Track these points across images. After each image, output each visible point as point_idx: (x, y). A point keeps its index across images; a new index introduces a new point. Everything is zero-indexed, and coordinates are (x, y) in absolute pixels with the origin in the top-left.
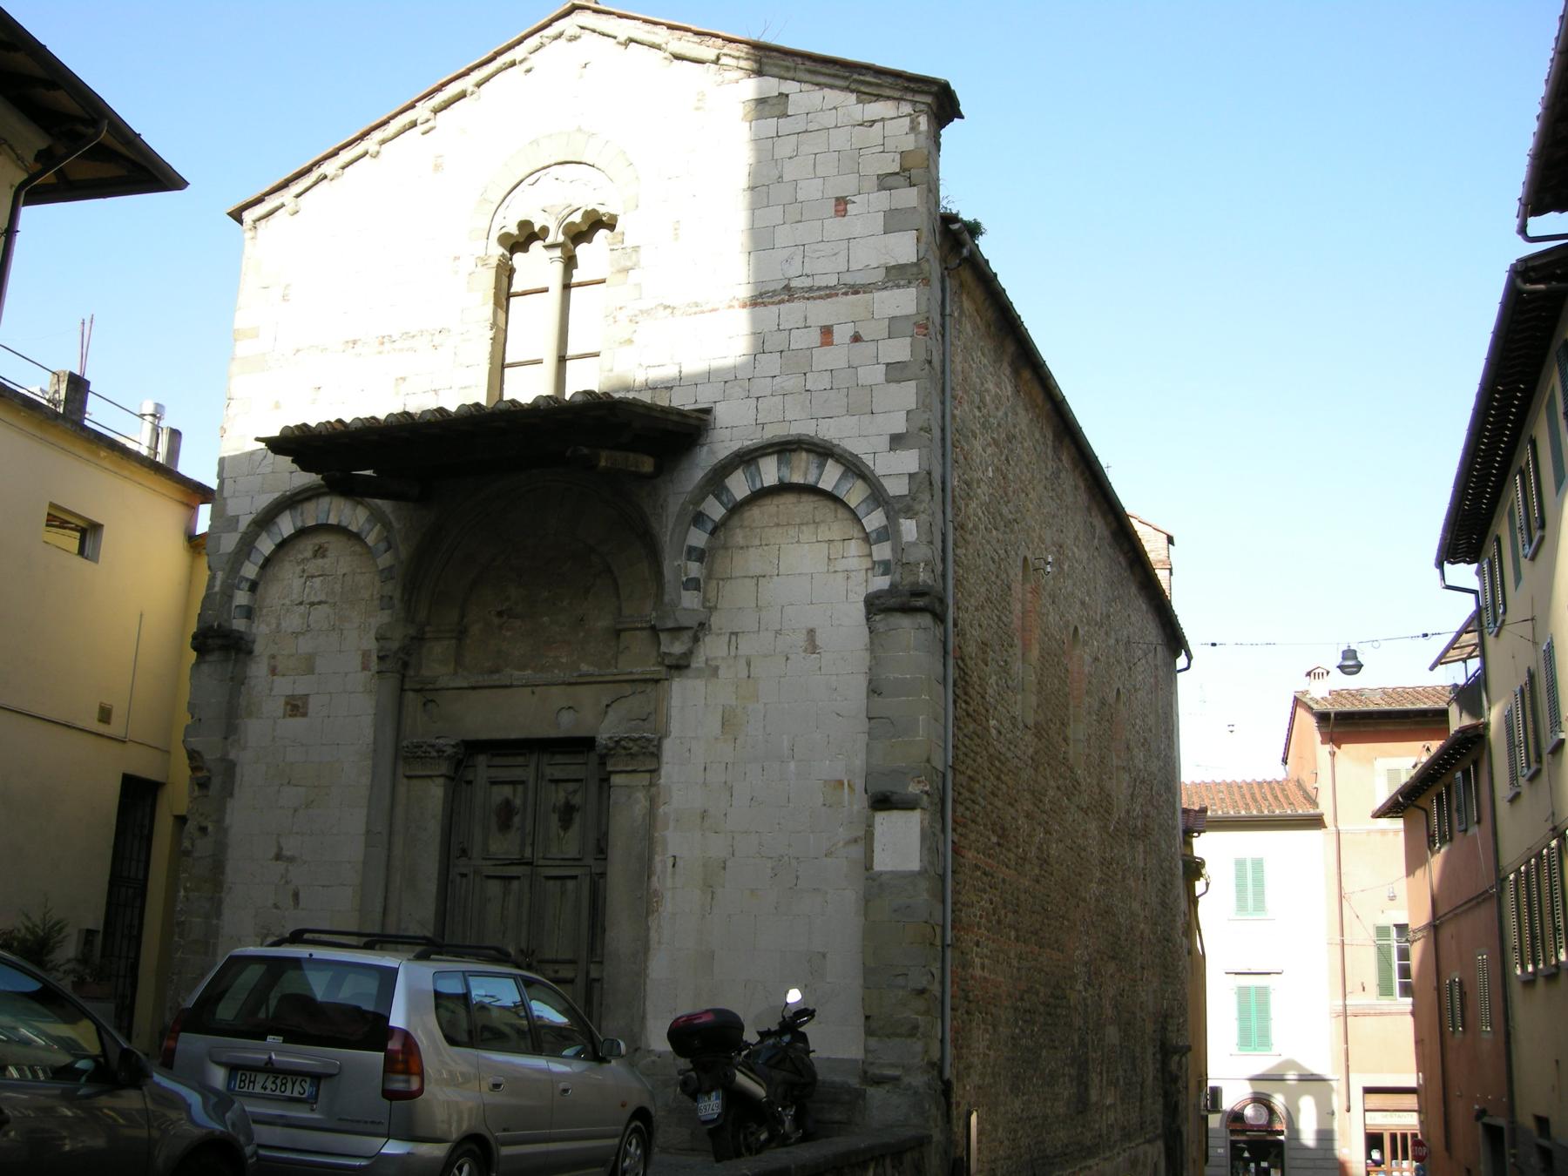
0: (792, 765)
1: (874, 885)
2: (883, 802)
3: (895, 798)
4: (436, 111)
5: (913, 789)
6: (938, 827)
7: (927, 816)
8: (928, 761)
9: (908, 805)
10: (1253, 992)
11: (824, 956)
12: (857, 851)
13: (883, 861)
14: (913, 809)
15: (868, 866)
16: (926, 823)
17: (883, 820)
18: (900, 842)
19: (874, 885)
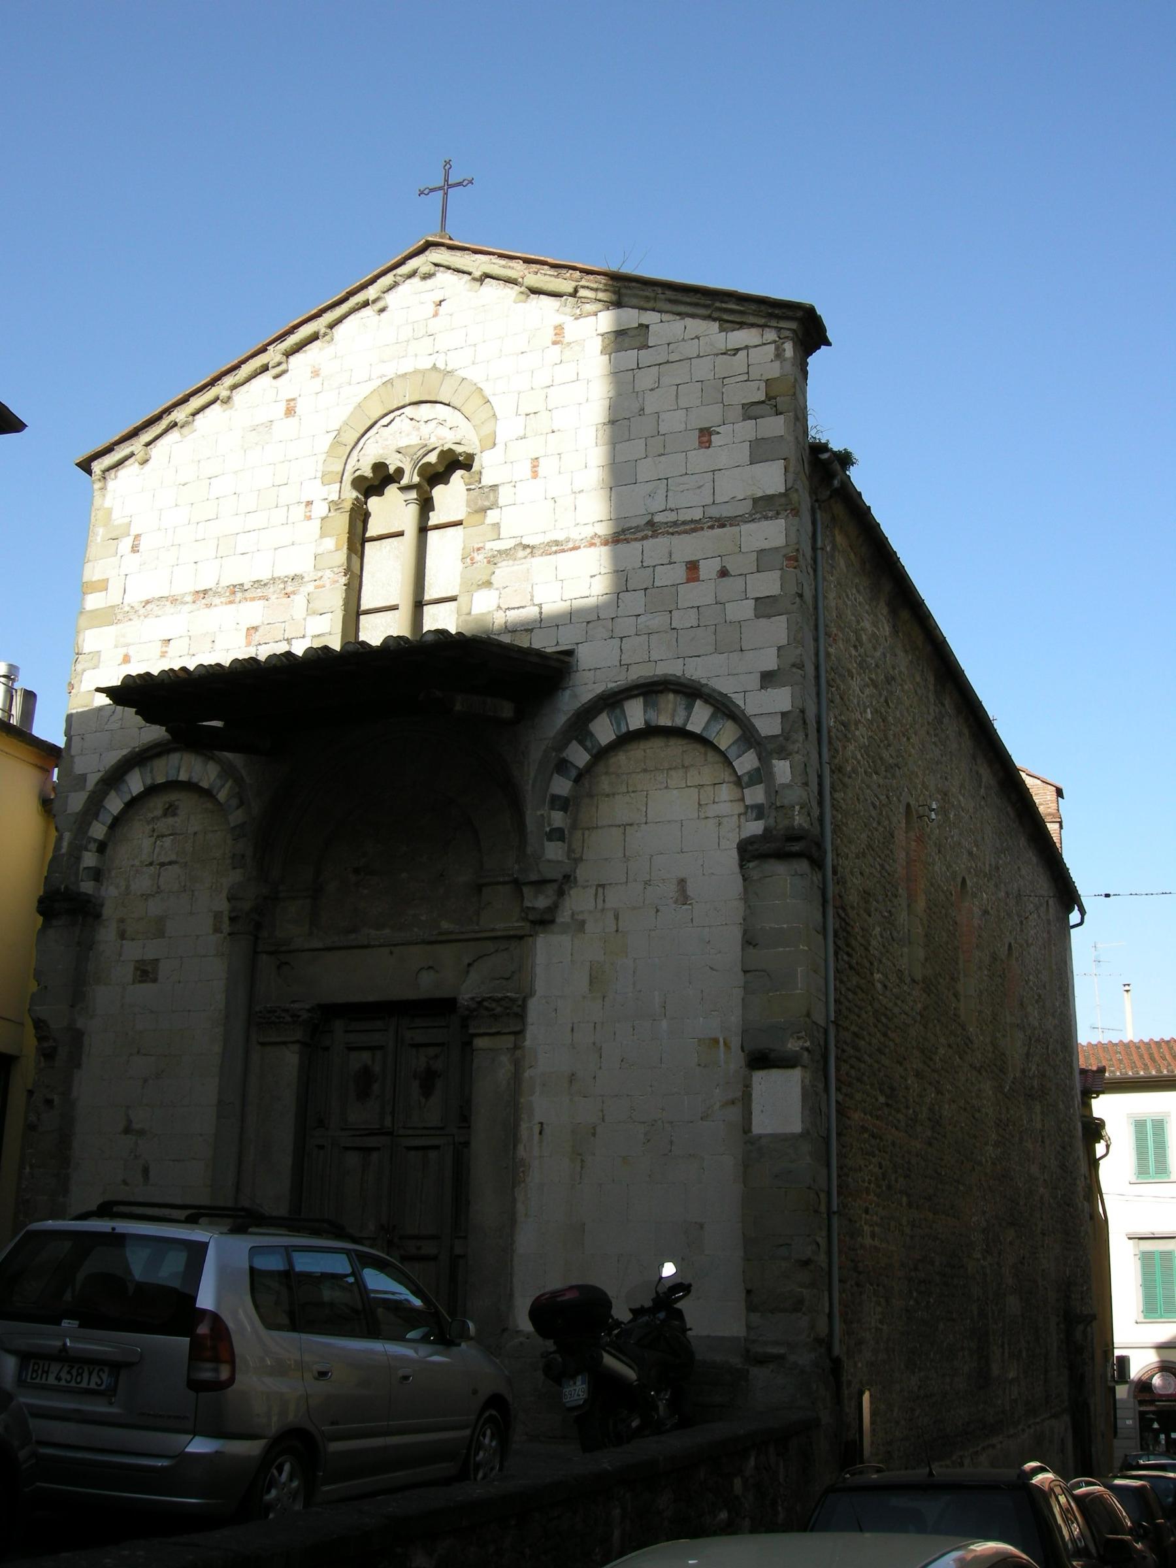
0: (664, 1024)
1: (754, 1150)
2: (760, 1060)
5: (793, 1045)
8: (808, 1015)
9: (786, 1062)
11: (701, 1226)
13: (762, 1125)
14: (793, 1066)
15: (747, 1129)
16: (807, 1081)
17: (765, 1082)
19: (754, 1150)
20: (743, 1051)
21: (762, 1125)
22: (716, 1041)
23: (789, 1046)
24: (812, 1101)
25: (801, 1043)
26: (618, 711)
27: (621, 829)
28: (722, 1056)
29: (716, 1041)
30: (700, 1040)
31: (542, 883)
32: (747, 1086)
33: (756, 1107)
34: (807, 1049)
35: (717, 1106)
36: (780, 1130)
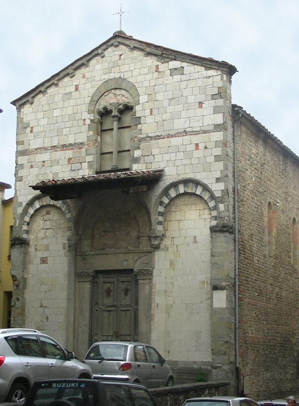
1: (213, 312)
2: (215, 288)
3: (218, 287)
5: (224, 284)
6: (232, 294)
9: (222, 288)
12: (209, 302)
14: (224, 290)
15: (212, 307)
18: (221, 299)
19: (213, 312)
22: (204, 282)
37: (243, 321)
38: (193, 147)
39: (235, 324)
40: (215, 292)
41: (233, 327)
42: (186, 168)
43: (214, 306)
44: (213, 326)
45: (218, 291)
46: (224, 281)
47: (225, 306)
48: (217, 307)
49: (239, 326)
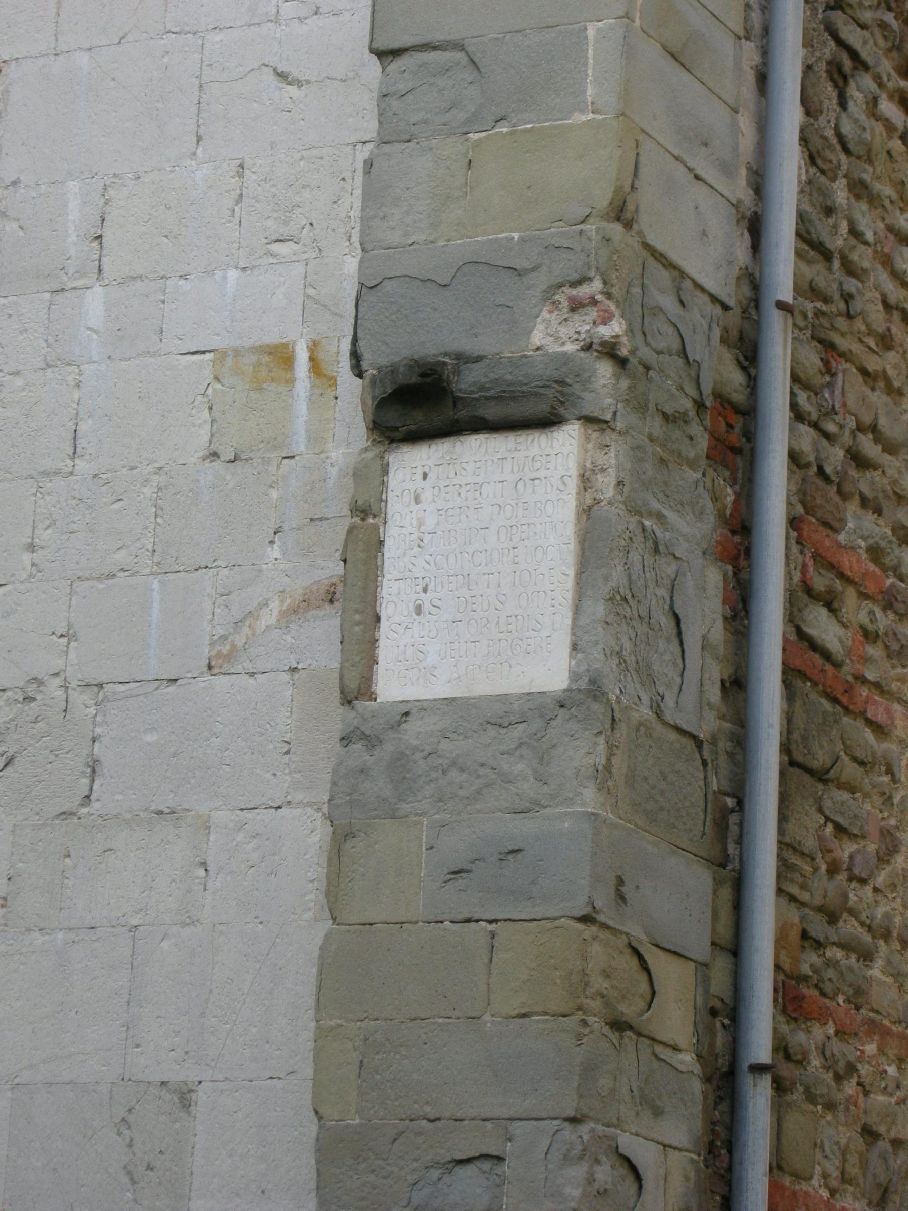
0: (95, 303)
1: (377, 757)
2: (421, 403)
3: (468, 381)
4: (676, 1049)
5: (552, 335)
6: (692, 529)
7: (613, 458)
8: (621, 212)
9: (526, 410)
10: (809, 272)
11: (185, 1097)
12: (320, 641)
13: (416, 666)
14: (547, 422)
15: (356, 689)
16: (606, 485)
17: (431, 480)
18: (498, 572)
19: (377, 757)
20: (358, 371)
21: (416, 666)
22: (282, 356)
23: (537, 337)
24: (612, 550)
25: (583, 324)
26: (791, 517)
27: (350, 147)
28: (302, 408)
29: (282, 356)
30: (221, 355)
31: (420, 776)
32: (367, 513)
33: (394, 597)
34: (609, 351)
35: (269, 617)
36: (485, 686)
37: (858, 996)
38: (405, 74)
39: (728, 1013)
40: (415, 469)
41: (676, 1018)
42: (28, 531)
43: (392, 686)
44: (355, 971)
45: (475, 449)
46: (549, 295)
47: (548, 669)
48: (440, 690)
49: (782, 1048)
